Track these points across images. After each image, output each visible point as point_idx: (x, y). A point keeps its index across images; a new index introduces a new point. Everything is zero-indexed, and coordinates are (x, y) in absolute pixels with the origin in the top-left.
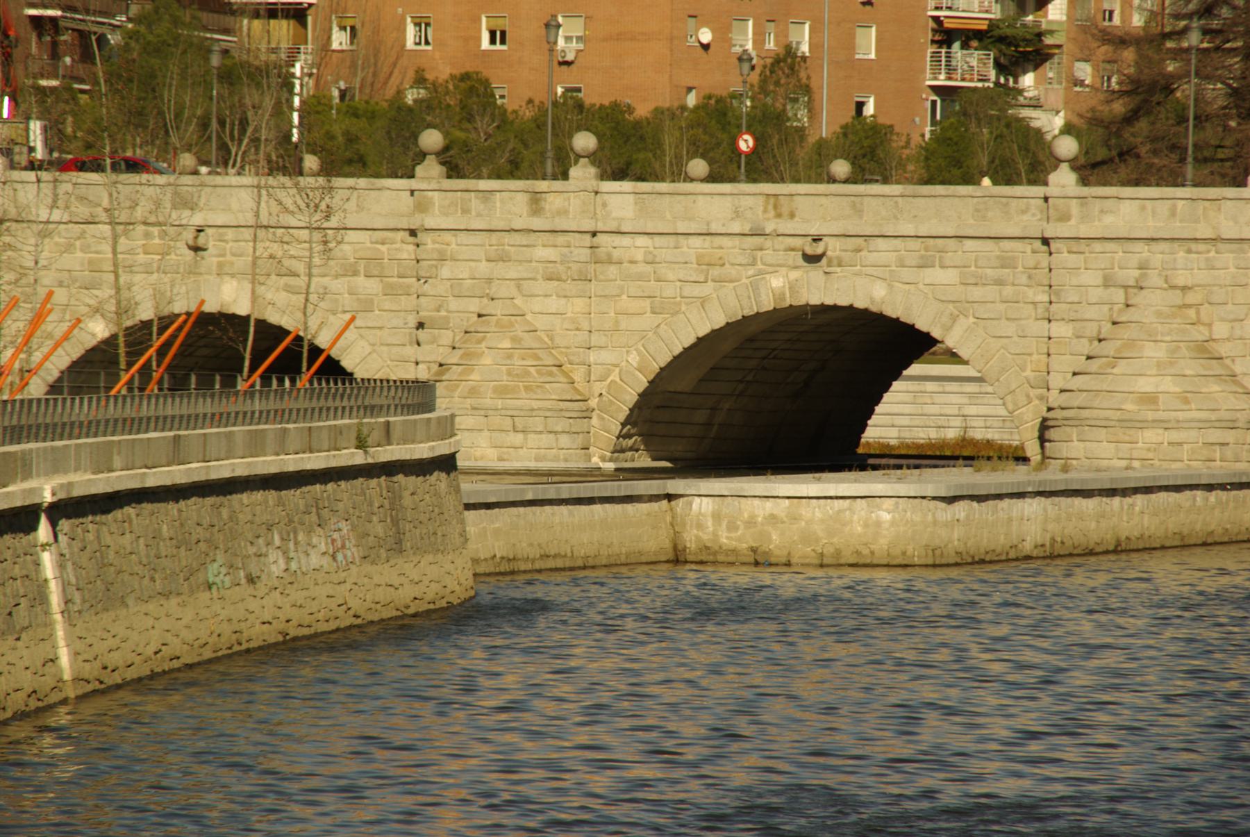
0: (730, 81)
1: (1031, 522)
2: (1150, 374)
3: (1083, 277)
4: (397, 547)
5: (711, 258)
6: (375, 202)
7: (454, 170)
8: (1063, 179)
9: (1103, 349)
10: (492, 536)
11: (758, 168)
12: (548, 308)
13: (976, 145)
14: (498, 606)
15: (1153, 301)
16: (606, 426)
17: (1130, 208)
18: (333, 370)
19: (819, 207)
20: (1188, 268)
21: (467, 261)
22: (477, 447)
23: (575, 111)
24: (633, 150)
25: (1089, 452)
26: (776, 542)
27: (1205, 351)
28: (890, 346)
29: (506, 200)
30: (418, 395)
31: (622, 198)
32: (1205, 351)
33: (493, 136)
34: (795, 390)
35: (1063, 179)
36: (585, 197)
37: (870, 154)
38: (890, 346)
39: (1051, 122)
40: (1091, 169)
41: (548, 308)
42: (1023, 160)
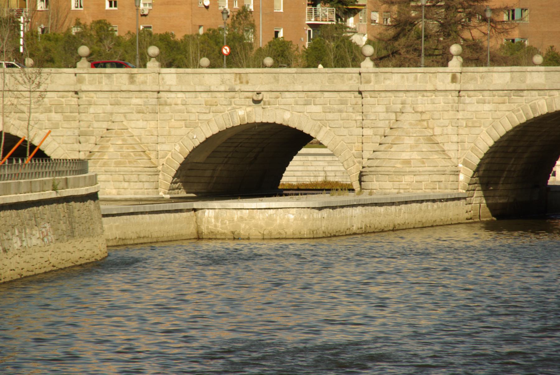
0: (219, 23)
1: (356, 218)
2: (407, 151)
3: (377, 108)
4: (72, 235)
5: (211, 103)
6: (60, 78)
7: (97, 63)
8: (367, 65)
9: (388, 138)
10: (113, 229)
11: (231, 62)
12: (138, 126)
13: (329, 51)
14: (119, 260)
15: (408, 118)
16: (166, 178)
17: (397, 77)
18: (41, 155)
19: (260, 79)
20: (423, 103)
21: (101, 105)
22: (107, 189)
23: (148, 37)
24: (175, 54)
25: (380, 187)
26: (243, 229)
27: (431, 140)
28: (293, 140)
29: (119, 77)
30: (80, 166)
31: (171, 76)
32: (431, 140)
33: (112, 51)
34: (251, 161)
35: (367, 65)
36: (155, 76)
37: (281, 55)
38: (293, 140)
39: (360, 40)
40: (379, 60)
41: (138, 126)
42: (348, 56)
